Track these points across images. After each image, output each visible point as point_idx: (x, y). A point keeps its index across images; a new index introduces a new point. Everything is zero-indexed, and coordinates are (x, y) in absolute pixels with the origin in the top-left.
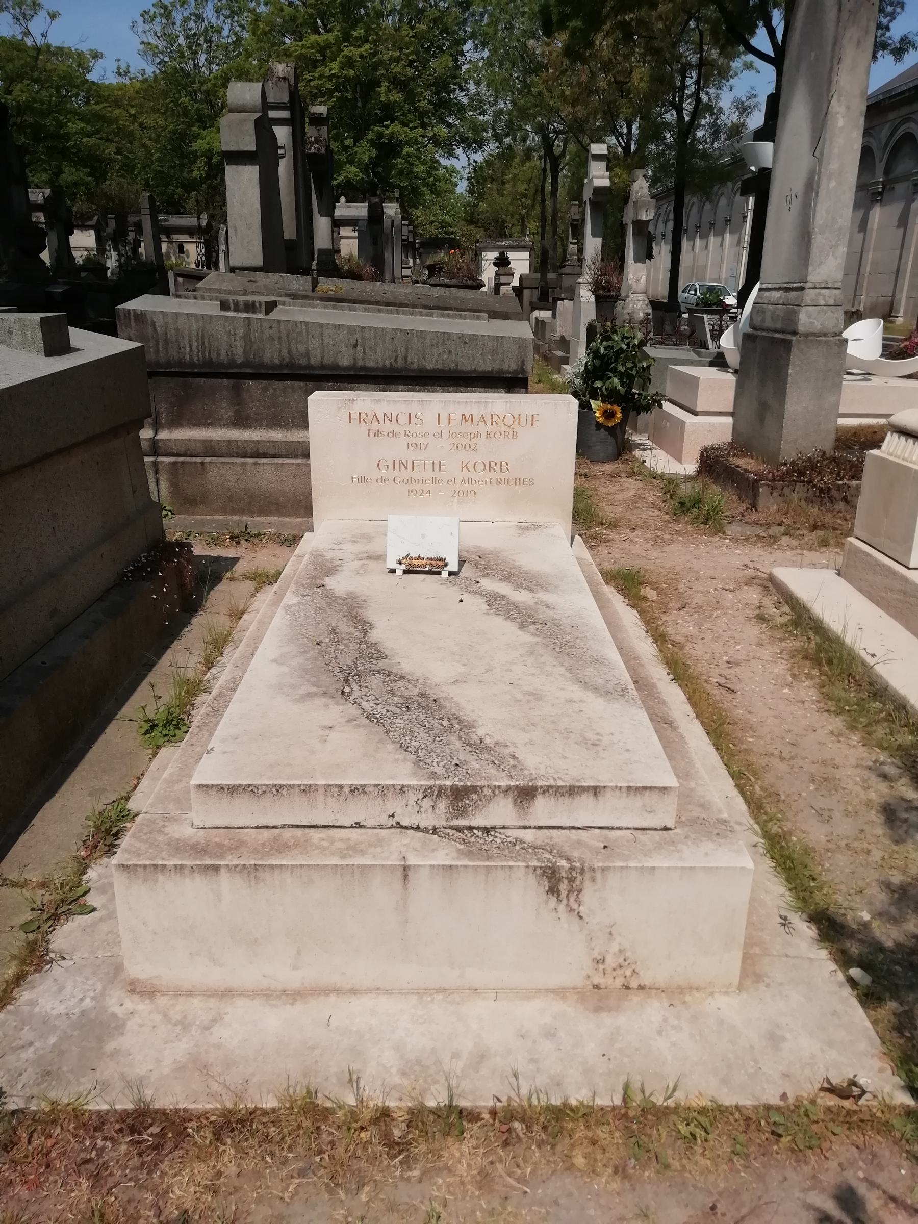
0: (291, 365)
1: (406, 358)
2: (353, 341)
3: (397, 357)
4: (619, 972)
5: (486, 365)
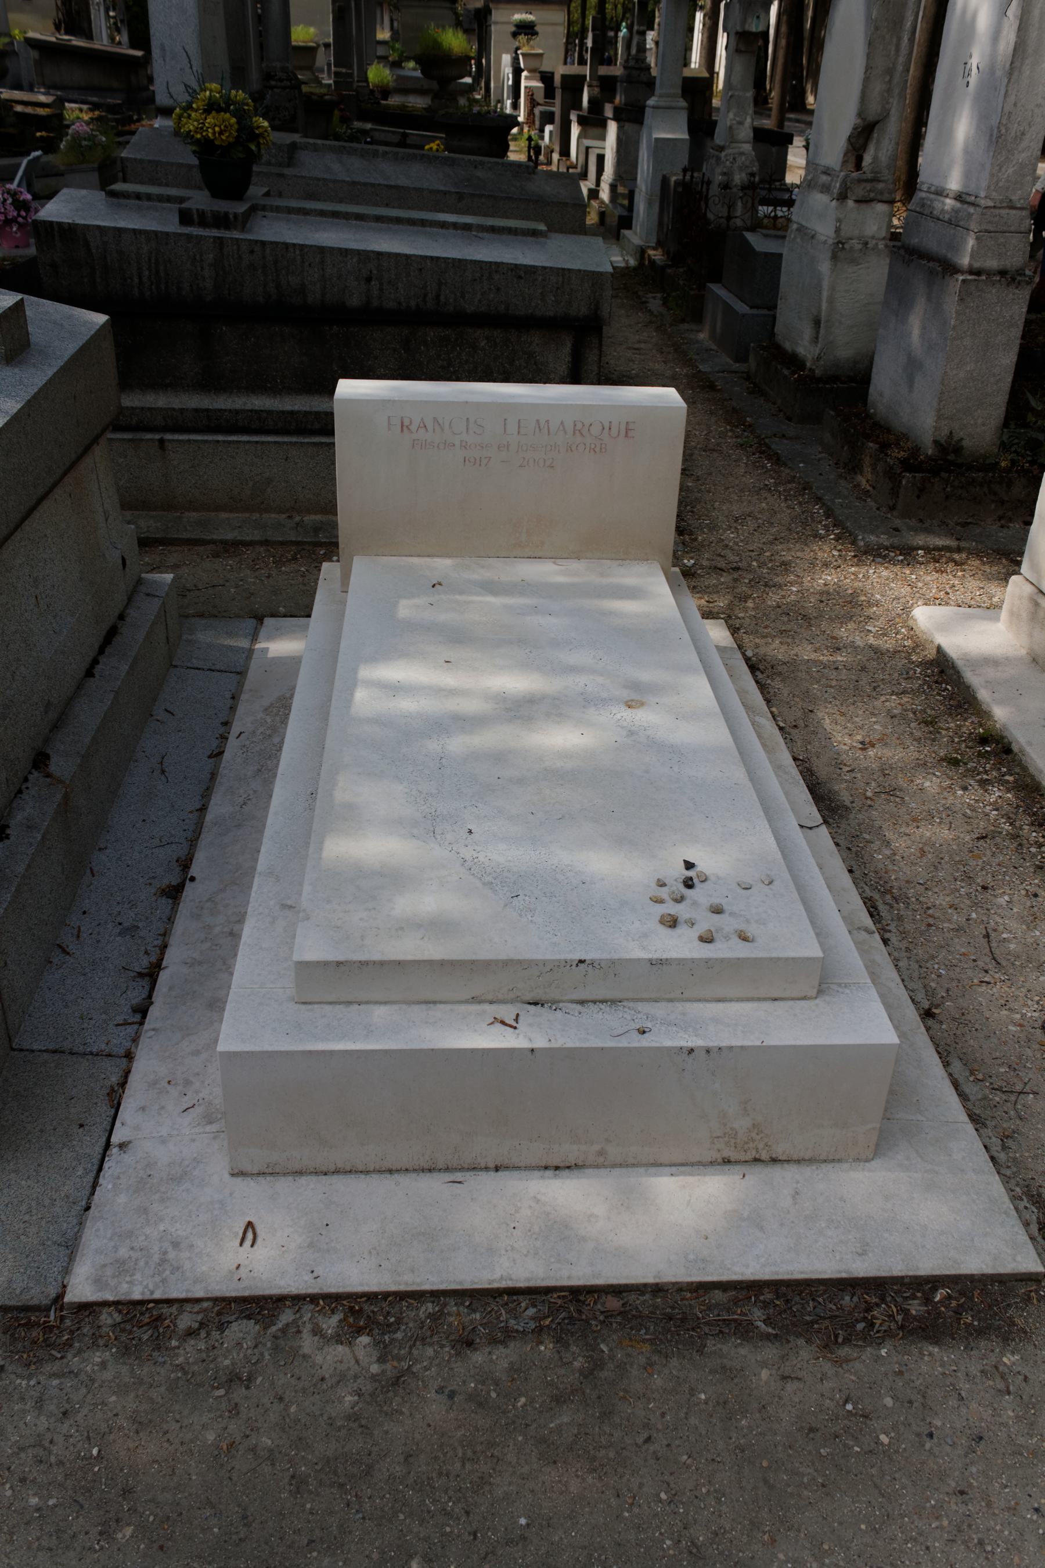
1: (438, 296)
3: (425, 295)
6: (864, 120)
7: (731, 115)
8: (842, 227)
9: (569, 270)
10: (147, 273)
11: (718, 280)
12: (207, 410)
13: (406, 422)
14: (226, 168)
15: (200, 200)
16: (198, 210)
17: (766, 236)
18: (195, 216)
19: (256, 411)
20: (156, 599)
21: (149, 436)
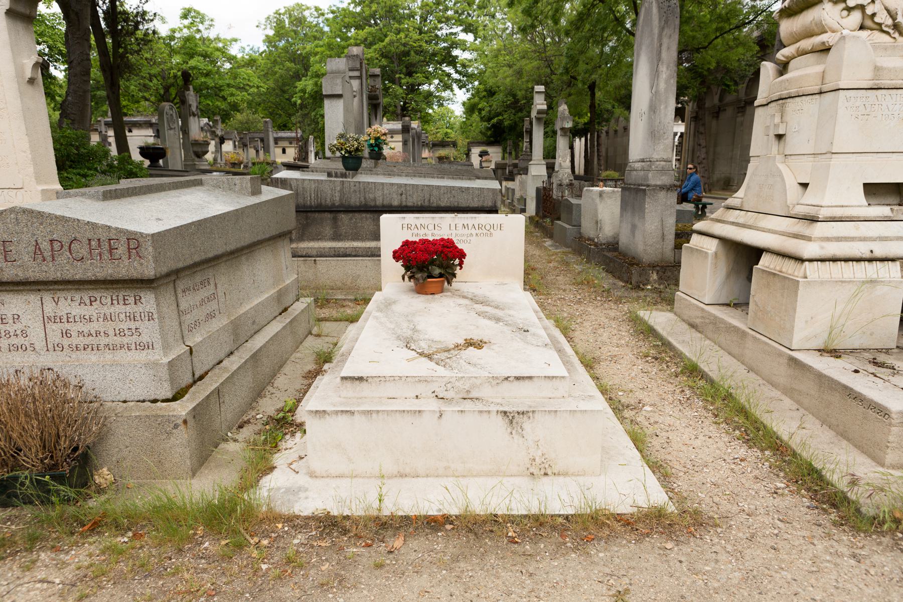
0: (366, 205)
2: (400, 192)
4: (543, 465)
5: (475, 204)
11: (559, 219)
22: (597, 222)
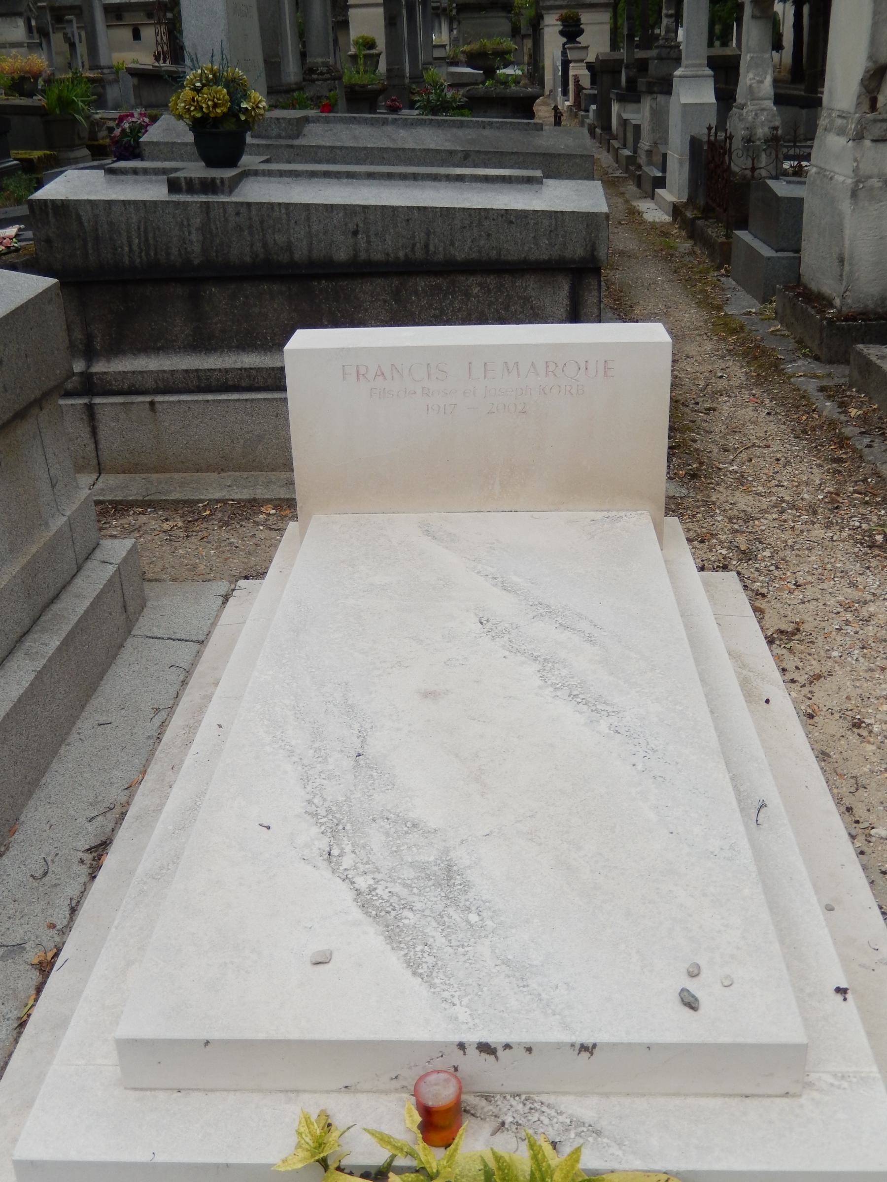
1: (427, 246)
2: (351, 226)
3: (414, 245)
6: (875, 62)
7: (751, 75)
8: (861, 166)
9: (562, 212)
10: (137, 241)
11: (743, 224)
12: (197, 371)
13: (362, 370)
14: (221, 138)
15: (196, 170)
16: (185, 178)
17: (789, 182)
18: (183, 184)
19: (245, 369)
20: (110, 567)
21: (140, 399)
22: (841, 260)
